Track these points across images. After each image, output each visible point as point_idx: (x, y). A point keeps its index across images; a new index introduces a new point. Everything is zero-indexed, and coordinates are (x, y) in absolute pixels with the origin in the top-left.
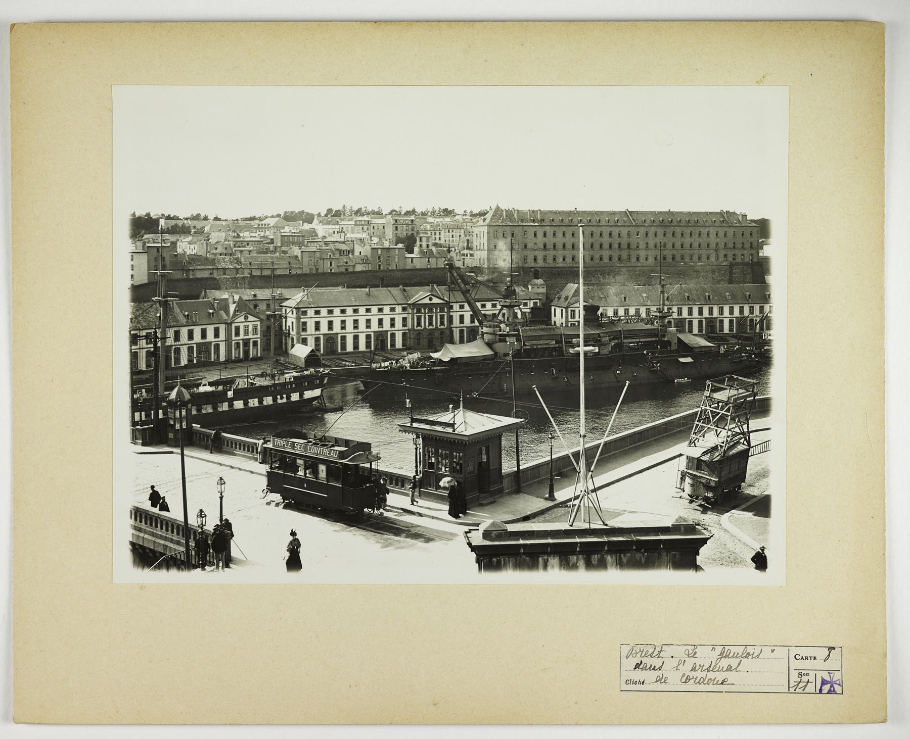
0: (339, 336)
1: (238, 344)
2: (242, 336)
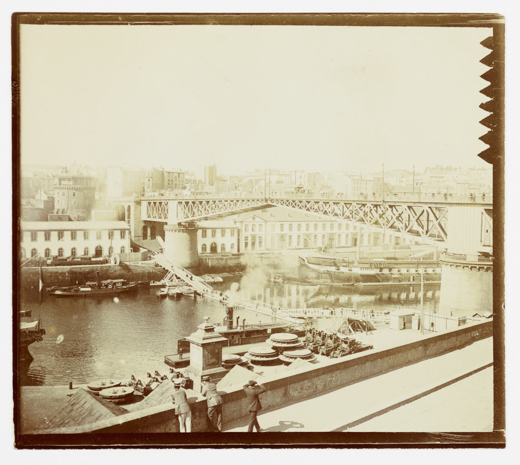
0: (288, 235)
1: (246, 238)
2: (303, 230)
